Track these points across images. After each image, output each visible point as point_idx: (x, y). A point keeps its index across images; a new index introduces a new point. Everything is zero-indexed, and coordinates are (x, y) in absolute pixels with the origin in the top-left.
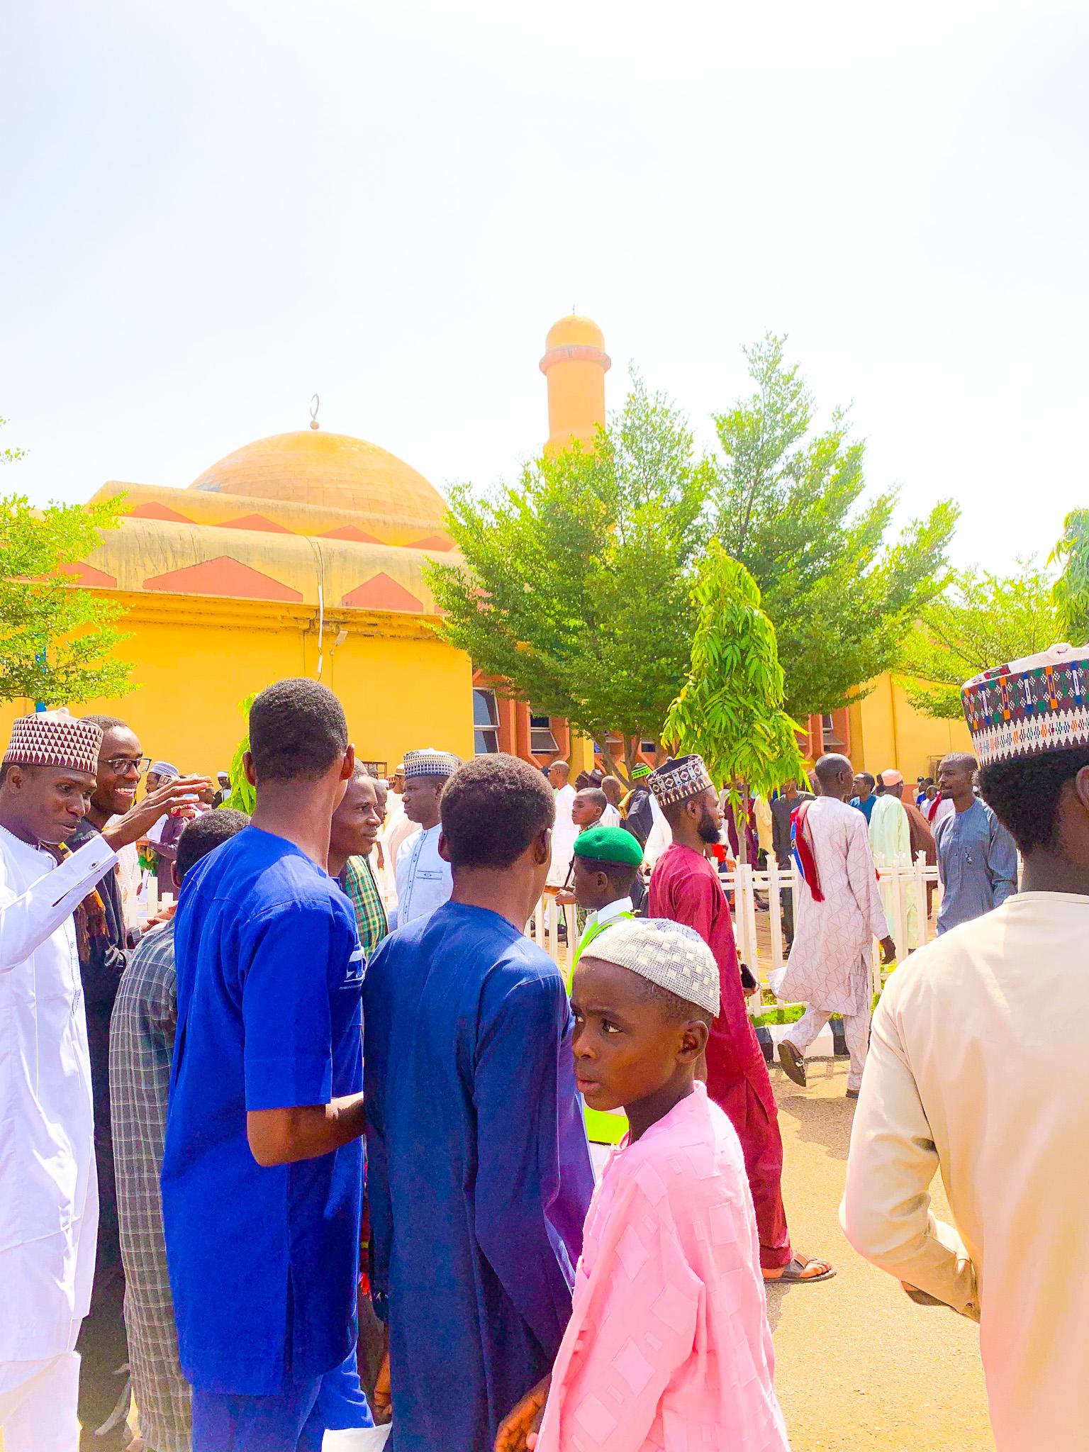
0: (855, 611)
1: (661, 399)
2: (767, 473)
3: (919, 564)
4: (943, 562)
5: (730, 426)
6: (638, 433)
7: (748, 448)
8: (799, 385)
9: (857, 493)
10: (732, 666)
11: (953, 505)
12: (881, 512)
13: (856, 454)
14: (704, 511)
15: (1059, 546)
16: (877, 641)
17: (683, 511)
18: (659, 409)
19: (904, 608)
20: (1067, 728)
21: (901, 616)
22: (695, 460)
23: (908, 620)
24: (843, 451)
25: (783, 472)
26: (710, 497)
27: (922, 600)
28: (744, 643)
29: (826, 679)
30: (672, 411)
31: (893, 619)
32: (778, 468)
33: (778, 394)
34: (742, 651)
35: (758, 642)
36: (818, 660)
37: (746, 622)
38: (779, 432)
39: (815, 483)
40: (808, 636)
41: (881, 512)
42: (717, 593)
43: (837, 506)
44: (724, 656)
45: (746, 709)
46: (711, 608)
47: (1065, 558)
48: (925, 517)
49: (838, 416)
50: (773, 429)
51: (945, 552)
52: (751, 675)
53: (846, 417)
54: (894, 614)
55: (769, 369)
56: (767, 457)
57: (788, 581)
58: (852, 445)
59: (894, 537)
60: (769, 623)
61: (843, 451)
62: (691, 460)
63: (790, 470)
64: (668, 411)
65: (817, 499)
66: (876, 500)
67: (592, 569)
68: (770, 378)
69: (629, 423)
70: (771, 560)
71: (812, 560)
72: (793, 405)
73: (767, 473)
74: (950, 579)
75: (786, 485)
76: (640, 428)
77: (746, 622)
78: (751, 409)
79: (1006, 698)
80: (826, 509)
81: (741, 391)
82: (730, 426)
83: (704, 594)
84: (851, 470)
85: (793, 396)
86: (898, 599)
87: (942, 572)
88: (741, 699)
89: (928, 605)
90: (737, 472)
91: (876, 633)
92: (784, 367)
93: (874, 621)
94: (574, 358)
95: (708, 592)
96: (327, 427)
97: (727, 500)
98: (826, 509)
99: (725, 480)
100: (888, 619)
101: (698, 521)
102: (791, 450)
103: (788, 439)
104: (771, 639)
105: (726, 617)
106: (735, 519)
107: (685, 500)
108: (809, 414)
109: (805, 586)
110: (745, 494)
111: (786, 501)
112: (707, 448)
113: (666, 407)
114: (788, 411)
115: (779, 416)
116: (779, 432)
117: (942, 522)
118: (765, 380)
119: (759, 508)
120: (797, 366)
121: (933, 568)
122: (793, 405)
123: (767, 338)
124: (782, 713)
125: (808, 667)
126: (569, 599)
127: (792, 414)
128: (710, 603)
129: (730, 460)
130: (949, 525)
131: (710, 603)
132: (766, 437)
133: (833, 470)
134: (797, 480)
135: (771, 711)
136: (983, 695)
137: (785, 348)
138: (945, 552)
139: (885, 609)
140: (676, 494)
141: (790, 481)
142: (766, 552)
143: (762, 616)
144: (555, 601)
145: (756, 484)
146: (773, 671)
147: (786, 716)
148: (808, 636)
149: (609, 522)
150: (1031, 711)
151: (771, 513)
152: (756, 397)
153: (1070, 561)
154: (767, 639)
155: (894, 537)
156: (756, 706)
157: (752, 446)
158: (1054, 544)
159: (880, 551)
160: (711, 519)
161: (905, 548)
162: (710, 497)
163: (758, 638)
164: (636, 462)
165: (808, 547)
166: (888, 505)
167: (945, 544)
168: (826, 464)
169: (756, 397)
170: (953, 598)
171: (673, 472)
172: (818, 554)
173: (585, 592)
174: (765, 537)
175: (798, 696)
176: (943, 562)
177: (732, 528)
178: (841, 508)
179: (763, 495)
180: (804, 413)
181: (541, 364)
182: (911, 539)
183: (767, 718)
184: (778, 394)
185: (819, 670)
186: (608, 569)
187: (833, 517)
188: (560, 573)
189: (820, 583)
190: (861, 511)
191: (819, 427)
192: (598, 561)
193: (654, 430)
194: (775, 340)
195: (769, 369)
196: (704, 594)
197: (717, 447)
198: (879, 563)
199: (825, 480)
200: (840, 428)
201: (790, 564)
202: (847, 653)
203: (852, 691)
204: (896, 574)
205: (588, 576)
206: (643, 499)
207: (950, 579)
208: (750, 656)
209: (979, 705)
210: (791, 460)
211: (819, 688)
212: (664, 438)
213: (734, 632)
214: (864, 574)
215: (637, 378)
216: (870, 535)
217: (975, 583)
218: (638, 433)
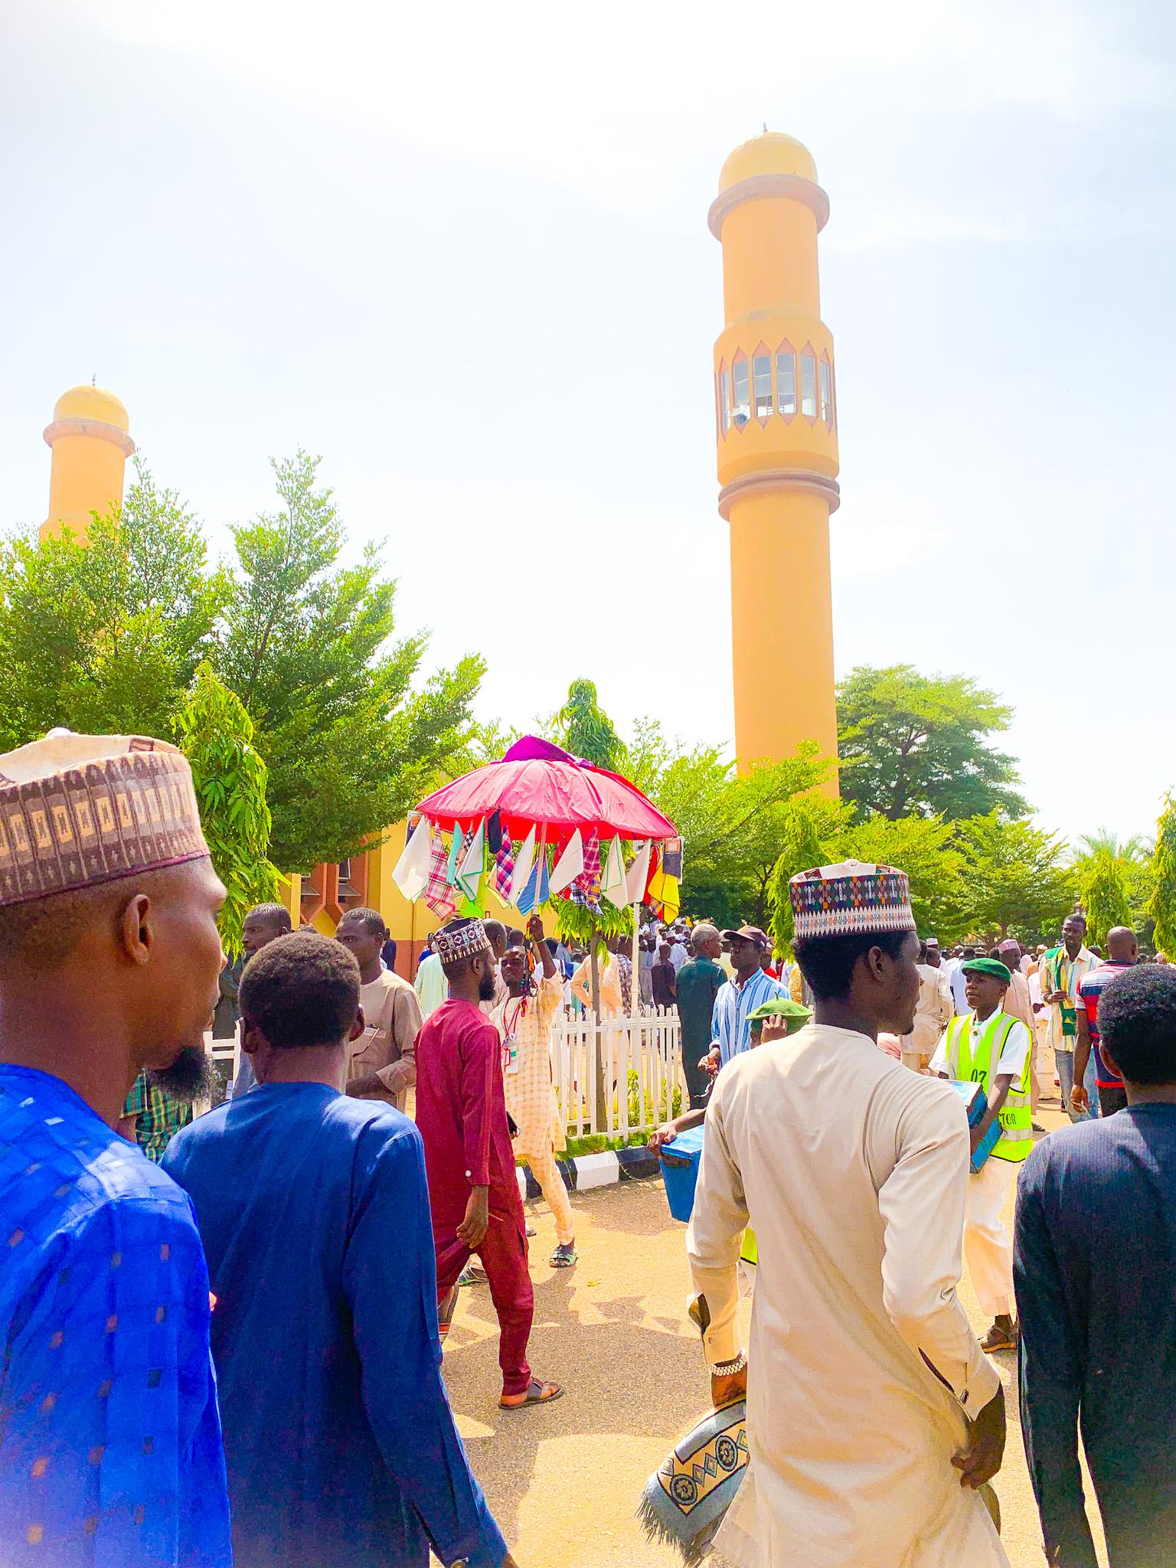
0: (375, 756)
1: (171, 499)
2: (289, 599)
3: (444, 714)
4: (467, 716)
5: (249, 543)
6: (141, 531)
7: (270, 568)
8: (331, 512)
9: (385, 634)
10: (212, 806)
11: (480, 661)
12: (409, 656)
13: (386, 593)
14: (214, 629)
15: (562, 712)
16: (393, 789)
17: (190, 623)
18: (168, 509)
19: (424, 759)
20: (845, 921)
21: (419, 767)
22: (208, 570)
23: (428, 770)
24: (374, 584)
25: (306, 599)
26: (222, 614)
27: (446, 750)
28: (228, 780)
29: (337, 825)
30: (184, 514)
31: (411, 768)
32: (301, 595)
33: (308, 518)
34: (227, 790)
35: (246, 781)
36: (330, 804)
37: (234, 757)
38: (304, 557)
39: (341, 615)
40: (321, 778)
41: (409, 656)
42: (202, 721)
43: (364, 645)
44: (204, 793)
45: (225, 854)
46: (193, 738)
47: (567, 724)
48: (451, 668)
49: (370, 551)
50: (298, 551)
51: (469, 706)
52: (232, 818)
53: (377, 555)
54: (414, 763)
55: (297, 486)
56: (290, 581)
57: (304, 716)
58: (382, 583)
59: (420, 684)
60: (260, 761)
61: (374, 584)
62: (202, 570)
63: (314, 599)
64: (178, 513)
65: (343, 633)
66: (404, 642)
67: (72, 677)
68: (299, 498)
69: (131, 519)
70: (289, 691)
71: (335, 697)
72: (322, 531)
73: (289, 599)
74: (473, 734)
75: (308, 613)
76: (143, 526)
77: (234, 757)
78: (275, 527)
79: (825, 894)
80: (351, 646)
81: (265, 507)
82: (249, 543)
83: (187, 720)
84: (380, 610)
85: (323, 523)
86: (419, 747)
87: (465, 725)
88: (221, 843)
89: (450, 758)
90: (255, 592)
91: (393, 780)
92: (315, 490)
93: (392, 769)
94: (87, 433)
95: (193, 720)
96: (98, 387)
97: (242, 620)
98: (351, 646)
99: (241, 599)
100: (407, 768)
101: (207, 638)
102: (316, 578)
103: (316, 565)
104: (261, 778)
105: (209, 751)
106: (251, 642)
107: (193, 613)
108: (338, 543)
109: (324, 724)
110: (263, 618)
111: (308, 632)
112: (221, 560)
113: (177, 508)
114: (317, 536)
115: (306, 541)
116: (304, 557)
117: (469, 674)
118: (294, 500)
119: (279, 635)
120: (329, 492)
121: (457, 720)
122: (322, 531)
123: (299, 457)
124: (265, 861)
125: (319, 811)
126: (40, 709)
127: (321, 540)
128: (193, 732)
129: (250, 578)
130: (474, 682)
131: (193, 732)
132: (290, 560)
133: (360, 606)
134: (321, 609)
135: (254, 858)
136: (809, 890)
137: (318, 472)
138: (469, 706)
139: (406, 757)
140: (182, 605)
141: (314, 611)
142: (284, 682)
143: (252, 752)
144: (21, 710)
145: (276, 608)
146: (260, 816)
147: (271, 865)
148: (321, 778)
149: (96, 625)
150: (841, 906)
151: (289, 641)
152: (282, 516)
153: (572, 728)
154: (258, 777)
155: (420, 684)
156: (236, 852)
157: (275, 569)
158: (558, 709)
159: (406, 695)
160: (222, 638)
161: (430, 697)
162: (222, 614)
163: (246, 776)
164: (138, 565)
165: (330, 683)
166: (417, 650)
167: (470, 699)
168: (354, 599)
169: (282, 516)
170: (476, 751)
171: (181, 580)
172: (340, 690)
173: (59, 703)
174: (283, 667)
175: (306, 841)
176: (467, 716)
177: (245, 652)
178: (369, 647)
179: (283, 622)
180: (333, 542)
181: (46, 431)
182: (438, 689)
183: (249, 866)
184: (308, 518)
185: (329, 817)
186: (92, 679)
187: (358, 656)
188: (31, 677)
189: (340, 722)
190: (389, 652)
191: (348, 559)
192: (80, 669)
193: (161, 532)
194: (307, 460)
195: (297, 486)
196: (187, 720)
197: (234, 561)
198: (403, 709)
199: (352, 614)
200: (372, 564)
201: (308, 699)
202: (362, 799)
203: (369, 838)
204: (419, 722)
205: (65, 684)
206: (142, 605)
207: (473, 734)
208: (234, 795)
209: (804, 896)
210: (315, 588)
211: (329, 834)
212: (172, 541)
213: (219, 767)
214: (388, 717)
215: (143, 471)
216: (396, 679)
217: (497, 738)
218: (141, 531)
